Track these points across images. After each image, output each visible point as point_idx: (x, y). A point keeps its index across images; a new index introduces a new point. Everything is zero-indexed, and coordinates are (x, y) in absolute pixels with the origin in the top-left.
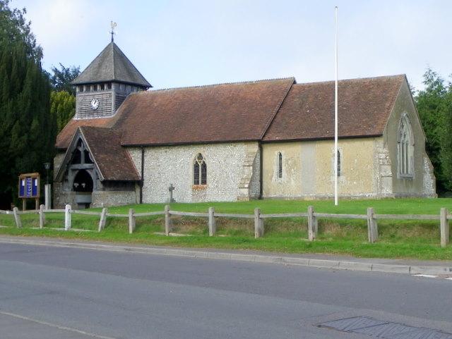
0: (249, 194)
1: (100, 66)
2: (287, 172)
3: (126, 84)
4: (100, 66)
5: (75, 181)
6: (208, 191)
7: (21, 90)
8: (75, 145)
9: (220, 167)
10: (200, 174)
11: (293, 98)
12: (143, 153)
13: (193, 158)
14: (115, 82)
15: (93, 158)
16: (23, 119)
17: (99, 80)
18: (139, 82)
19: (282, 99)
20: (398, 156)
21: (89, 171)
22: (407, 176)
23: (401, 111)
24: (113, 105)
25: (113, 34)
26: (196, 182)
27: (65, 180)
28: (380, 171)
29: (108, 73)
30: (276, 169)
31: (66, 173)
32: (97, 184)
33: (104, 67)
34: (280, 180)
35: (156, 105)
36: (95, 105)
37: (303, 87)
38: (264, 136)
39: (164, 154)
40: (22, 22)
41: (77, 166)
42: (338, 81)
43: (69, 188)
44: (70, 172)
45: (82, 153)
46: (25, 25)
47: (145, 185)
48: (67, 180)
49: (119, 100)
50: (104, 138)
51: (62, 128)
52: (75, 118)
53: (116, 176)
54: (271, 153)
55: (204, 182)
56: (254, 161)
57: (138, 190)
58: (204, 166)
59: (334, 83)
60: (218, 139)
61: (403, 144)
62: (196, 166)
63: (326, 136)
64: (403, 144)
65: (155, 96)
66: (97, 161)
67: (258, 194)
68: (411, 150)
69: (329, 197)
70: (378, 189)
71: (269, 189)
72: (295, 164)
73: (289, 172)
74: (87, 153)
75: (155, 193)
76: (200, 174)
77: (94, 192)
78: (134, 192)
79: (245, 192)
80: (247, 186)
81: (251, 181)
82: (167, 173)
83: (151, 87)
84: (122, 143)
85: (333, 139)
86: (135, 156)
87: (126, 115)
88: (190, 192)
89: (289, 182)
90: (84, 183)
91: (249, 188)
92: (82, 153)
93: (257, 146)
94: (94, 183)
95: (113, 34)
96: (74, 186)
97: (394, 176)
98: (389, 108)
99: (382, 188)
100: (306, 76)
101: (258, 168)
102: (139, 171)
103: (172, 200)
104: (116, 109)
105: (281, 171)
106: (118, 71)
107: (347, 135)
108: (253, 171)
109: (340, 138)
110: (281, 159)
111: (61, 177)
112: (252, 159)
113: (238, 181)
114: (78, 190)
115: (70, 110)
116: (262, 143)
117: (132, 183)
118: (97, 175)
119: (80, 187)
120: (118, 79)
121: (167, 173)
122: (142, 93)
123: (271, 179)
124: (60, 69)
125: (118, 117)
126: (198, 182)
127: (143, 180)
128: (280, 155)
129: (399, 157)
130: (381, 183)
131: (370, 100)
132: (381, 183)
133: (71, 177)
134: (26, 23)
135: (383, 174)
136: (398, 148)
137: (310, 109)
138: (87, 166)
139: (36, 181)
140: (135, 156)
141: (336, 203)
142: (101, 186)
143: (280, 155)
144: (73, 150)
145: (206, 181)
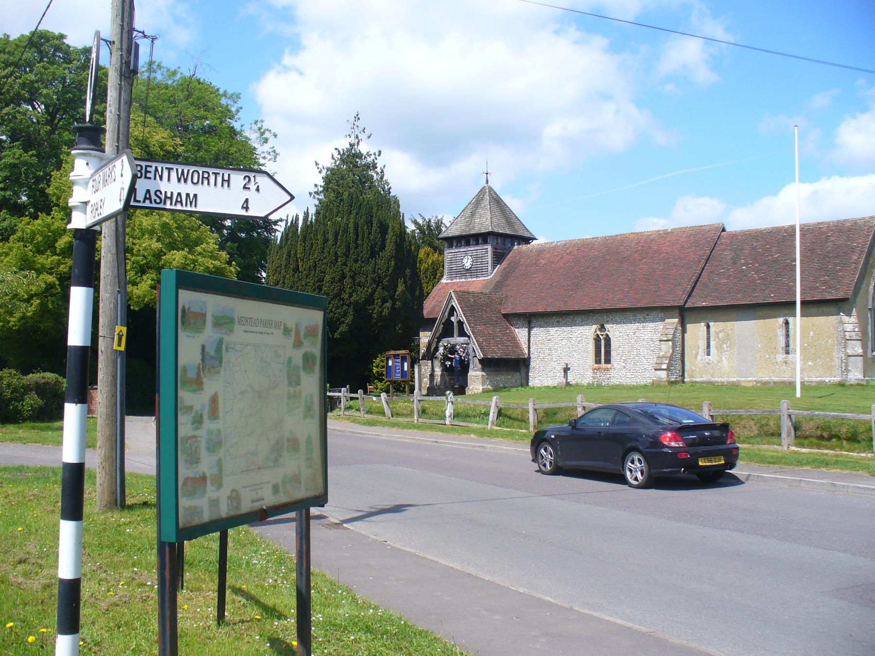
1: (473, 214)
2: (717, 348)
4: (473, 214)
6: (612, 373)
7: (383, 247)
8: (446, 314)
10: (603, 351)
11: (723, 250)
12: (683, 324)
15: (468, 329)
16: (385, 281)
17: (473, 232)
18: (521, 233)
19: (708, 252)
24: (490, 263)
26: (598, 361)
29: (484, 222)
30: (703, 344)
33: (477, 216)
35: (543, 262)
36: (468, 263)
37: (734, 236)
38: (686, 302)
40: (375, 166)
42: (800, 226)
45: (455, 324)
46: (378, 170)
47: (532, 364)
49: (498, 258)
51: (428, 294)
52: (444, 281)
54: (696, 331)
55: (608, 361)
56: (674, 335)
57: (523, 371)
58: (608, 340)
59: (793, 228)
60: (625, 306)
62: (597, 340)
63: (771, 300)
65: (541, 251)
69: (774, 383)
71: (693, 371)
72: (728, 338)
73: (719, 348)
74: (460, 323)
75: (543, 374)
76: (603, 351)
78: (518, 374)
80: (664, 367)
81: (670, 360)
83: (535, 239)
85: (794, 303)
86: (521, 333)
87: (505, 276)
88: (590, 373)
89: (720, 361)
92: (455, 324)
102: (525, 347)
103: (568, 384)
104: (494, 267)
105: (708, 346)
106: (495, 220)
107: (758, 298)
109: (802, 303)
112: (672, 332)
115: (436, 272)
122: (524, 247)
123: (696, 357)
124: (187, 307)
125: (497, 279)
126: (600, 360)
130: (847, 366)
131: (829, 252)
134: (379, 166)
135: (850, 352)
137: (746, 264)
138: (462, 339)
139: (406, 364)
141: (798, 395)
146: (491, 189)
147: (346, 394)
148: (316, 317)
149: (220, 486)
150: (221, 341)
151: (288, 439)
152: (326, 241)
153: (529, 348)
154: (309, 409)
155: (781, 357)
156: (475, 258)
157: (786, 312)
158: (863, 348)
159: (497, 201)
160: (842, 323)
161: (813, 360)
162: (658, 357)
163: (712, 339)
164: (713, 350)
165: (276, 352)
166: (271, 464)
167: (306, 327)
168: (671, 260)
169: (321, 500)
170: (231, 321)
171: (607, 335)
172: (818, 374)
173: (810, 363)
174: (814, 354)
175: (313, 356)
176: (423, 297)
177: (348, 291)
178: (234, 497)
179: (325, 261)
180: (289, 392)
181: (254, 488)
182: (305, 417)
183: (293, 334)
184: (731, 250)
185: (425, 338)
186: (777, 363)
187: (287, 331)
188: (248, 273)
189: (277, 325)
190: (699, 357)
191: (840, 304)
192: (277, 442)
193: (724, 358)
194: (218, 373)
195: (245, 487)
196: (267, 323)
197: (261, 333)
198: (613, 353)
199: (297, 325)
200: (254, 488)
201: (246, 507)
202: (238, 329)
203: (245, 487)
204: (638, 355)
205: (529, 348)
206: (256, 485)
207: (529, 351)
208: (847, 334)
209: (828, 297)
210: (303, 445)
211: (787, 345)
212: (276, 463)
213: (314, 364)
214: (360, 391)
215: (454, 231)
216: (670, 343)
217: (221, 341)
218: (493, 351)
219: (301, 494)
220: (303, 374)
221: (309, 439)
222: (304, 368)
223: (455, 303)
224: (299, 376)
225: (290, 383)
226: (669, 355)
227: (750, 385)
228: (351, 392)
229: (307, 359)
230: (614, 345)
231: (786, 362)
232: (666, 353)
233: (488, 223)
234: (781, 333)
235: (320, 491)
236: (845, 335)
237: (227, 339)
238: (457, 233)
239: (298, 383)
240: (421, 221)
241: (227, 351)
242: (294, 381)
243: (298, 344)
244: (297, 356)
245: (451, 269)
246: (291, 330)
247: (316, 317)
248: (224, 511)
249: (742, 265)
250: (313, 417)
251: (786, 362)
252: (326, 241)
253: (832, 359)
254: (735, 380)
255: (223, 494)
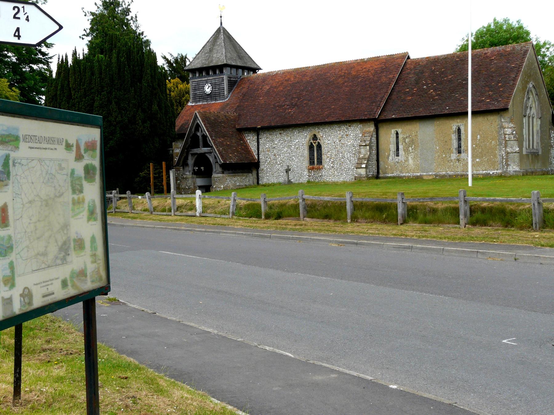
0: (366, 173)
1: (211, 51)
2: (404, 150)
3: (237, 67)
4: (211, 51)
5: (195, 165)
8: (193, 130)
9: (336, 148)
10: (315, 155)
13: (308, 139)
14: (226, 65)
17: (212, 64)
18: (249, 65)
20: (524, 130)
21: (208, 155)
22: (532, 151)
23: (527, 82)
25: (221, 17)
26: (311, 162)
27: (185, 164)
28: (506, 147)
29: (220, 57)
30: (393, 147)
31: (186, 158)
32: (216, 168)
33: (215, 51)
34: (397, 159)
36: (208, 89)
37: (417, 62)
39: (279, 135)
41: (196, 151)
43: (189, 172)
44: (190, 157)
45: (200, 137)
47: (262, 167)
48: (187, 165)
49: (232, 84)
50: (220, 123)
52: (190, 104)
53: (233, 159)
54: (388, 135)
55: (320, 162)
56: (371, 140)
57: (255, 172)
58: (319, 146)
61: (529, 117)
62: (311, 147)
63: (446, 112)
64: (529, 117)
66: (215, 145)
67: (375, 174)
68: (537, 123)
70: (503, 166)
71: (386, 168)
72: (412, 142)
73: (406, 150)
74: (204, 137)
75: (271, 173)
76: (315, 155)
77: (214, 175)
78: (250, 174)
79: (363, 172)
80: (364, 166)
81: (368, 161)
82: (282, 154)
83: (260, 69)
84: (237, 127)
85: (467, 113)
86: (251, 140)
88: (306, 172)
89: (407, 160)
90: (204, 169)
91: (366, 168)
93: (373, 125)
94: (214, 166)
95: (221, 17)
96: (194, 170)
97: (520, 152)
98: (515, 80)
99: (508, 165)
100: (419, 51)
101: (374, 148)
102: (255, 154)
103: (289, 182)
105: (398, 149)
108: (370, 151)
109: (473, 113)
110: (397, 137)
111: (181, 162)
112: (369, 139)
113: (355, 161)
114: (198, 174)
116: (378, 123)
117: (249, 166)
118: (216, 154)
119: (199, 170)
120: (229, 62)
121: (282, 154)
123: (388, 158)
126: (314, 162)
127: (259, 162)
128: (397, 134)
129: (525, 131)
130: (507, 161)
132: (507, 161)
133: (191, 161)
135: (509, 150)
136: (524, 121)
137: (427, 84)
138: (205, 150)
140: (251, 140)
142: (220, 170)
143: (397, 134)
144: (191, 135)
145: (321, 162)
146: (224, 30)
147: (116, 195)
148: (93, 134)
149: (13, 285)
150: (7, 157)
151: (75, 240)
152: (93, 74)
153: (258, 155)
154: (92, 213)
155: (454, 156)
156: (214, 86)
157: (459, 121)
158: (519, 147)
159: (229, 38)
160: (502, 127)
161: (480, 158)
162: (359, 159)
163: (400, 144)
164: (401, 152)
165: (60, 165)
166: (59, 262)
167: (86, 143)
168: (367, 82)
169: (104, 290)
170: (17, 139)
171: (319, 143)
172: (484, 168)
173: (478, 160)
174: (481, 153)
175: (94, 168)
176: (175, 116)
177: (114, 114)
178: (27, 295)
179: (93, 91)
180: (73, 199)
181: (44, 284)
182: (89, 220)
183: (74, 148)
184: (414, 73)
185: (177, 149)
186: (451, 161)
187: (68, 146)
188: (27, 96)
189: (59, 142)
190: (390, 158)
191: (502, 113)
192: (65, 243)
193: (410, 158)
194: (6, 185)
195: (37, 284)
196: (50, 140)
197: (46, 149)
198: (324, 157)
199: (77, 141)
200: (44, 284)
201: (38, 302)
202: (23, 146)
203: (37, 284)
204: (343, 157)
205: (258, 155)
206: (48, 281)
207: (258, 157)
208: (507, 136)
209: (493, 108)
210: (88, 244)
211: (460, 146)
212: (64, 261)
213: (94, 174)
214: (128, 192)
215: (197, 65)
216: (368, 147)
217: (7, 157)
218: (231, 158)
219: (88, 285)
220: (85, 183)
221: (93, 239)
222: (85, 178)
223: (200, 121)
224: (81, 186)
225: (74, 191)
226: (367, 156)
227: (431, 178)
228: (120, 193)
229: (88, 170)
230: (324, 150)
231: (458, 160)
232: (365, 155)
233: (223, 57)
234: (454, 137)
235: (103, 283)
236: (505, 138)
237: (13, 155)
238: (199, 66)
239: (81, 191)
240: (169, 58)
241: (14, 165)
242: (77, 189)
243: (79, 157)
244: (79, 168)
245: (195, 95)
246: (72, 146)
247: (93, 134)
248: (17, 308)
249: (424, 85)
250: (95, 220)
251: (458, 160)
252: (93, 74)
253: (495, 156)
254: (419, 174)
255: (16, 293)
